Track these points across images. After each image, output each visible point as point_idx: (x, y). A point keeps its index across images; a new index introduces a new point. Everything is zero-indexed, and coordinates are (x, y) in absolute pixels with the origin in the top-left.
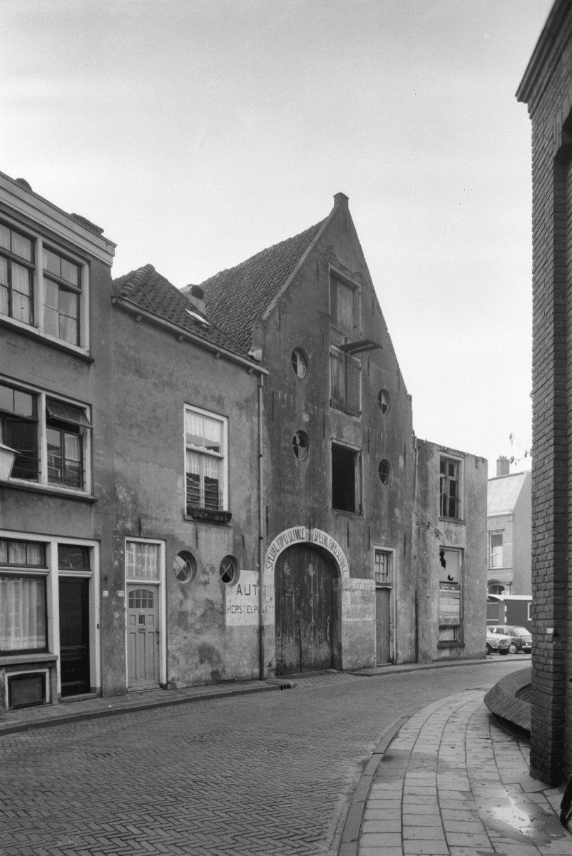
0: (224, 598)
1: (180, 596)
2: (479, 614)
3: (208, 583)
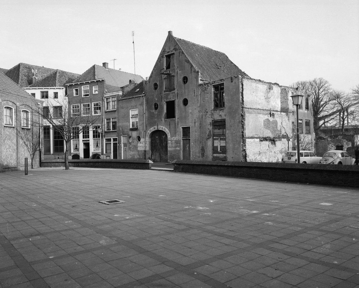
2: (236, 147)
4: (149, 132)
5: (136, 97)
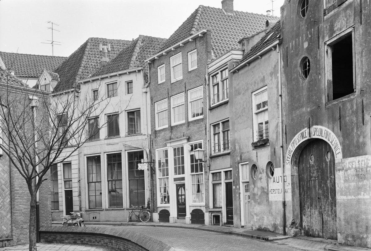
0: (268, 186)
1: (253, 186)
3: (262, 178)
4: (292, 147)
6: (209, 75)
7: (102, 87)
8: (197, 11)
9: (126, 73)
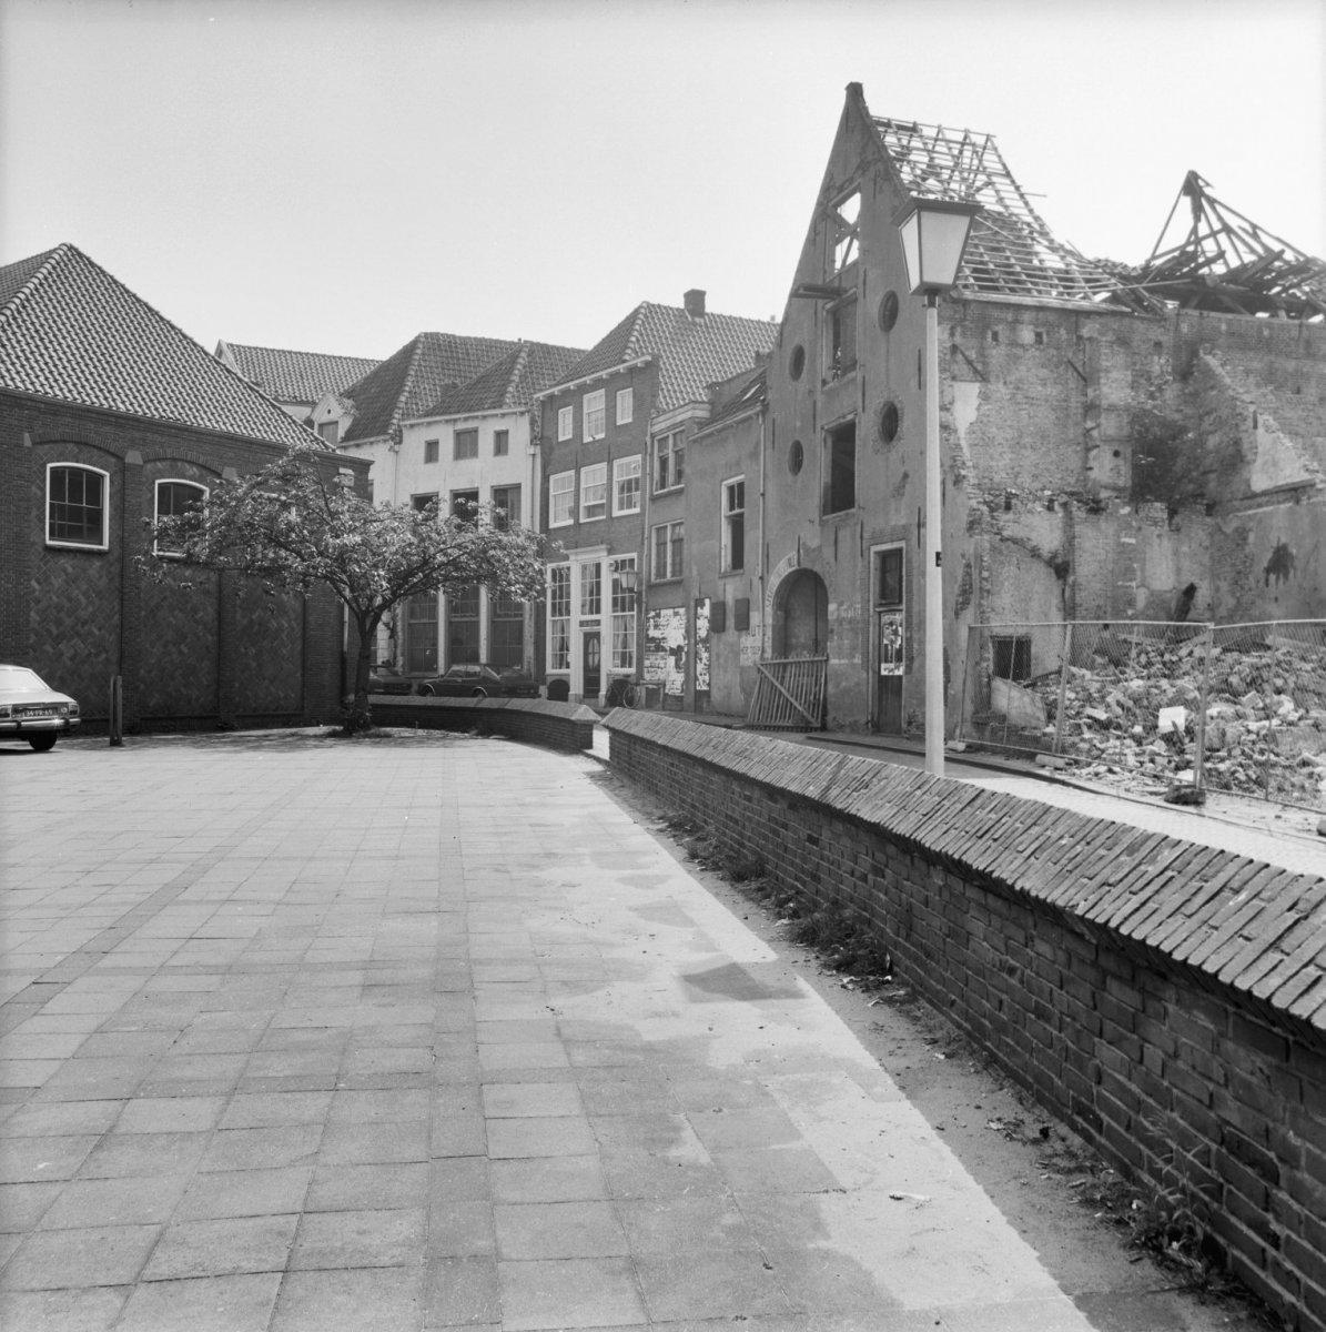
5: (738, 423)
6: (653, 436)
7: (445, 435)
8: (636, 312)
9: (497, 415)
